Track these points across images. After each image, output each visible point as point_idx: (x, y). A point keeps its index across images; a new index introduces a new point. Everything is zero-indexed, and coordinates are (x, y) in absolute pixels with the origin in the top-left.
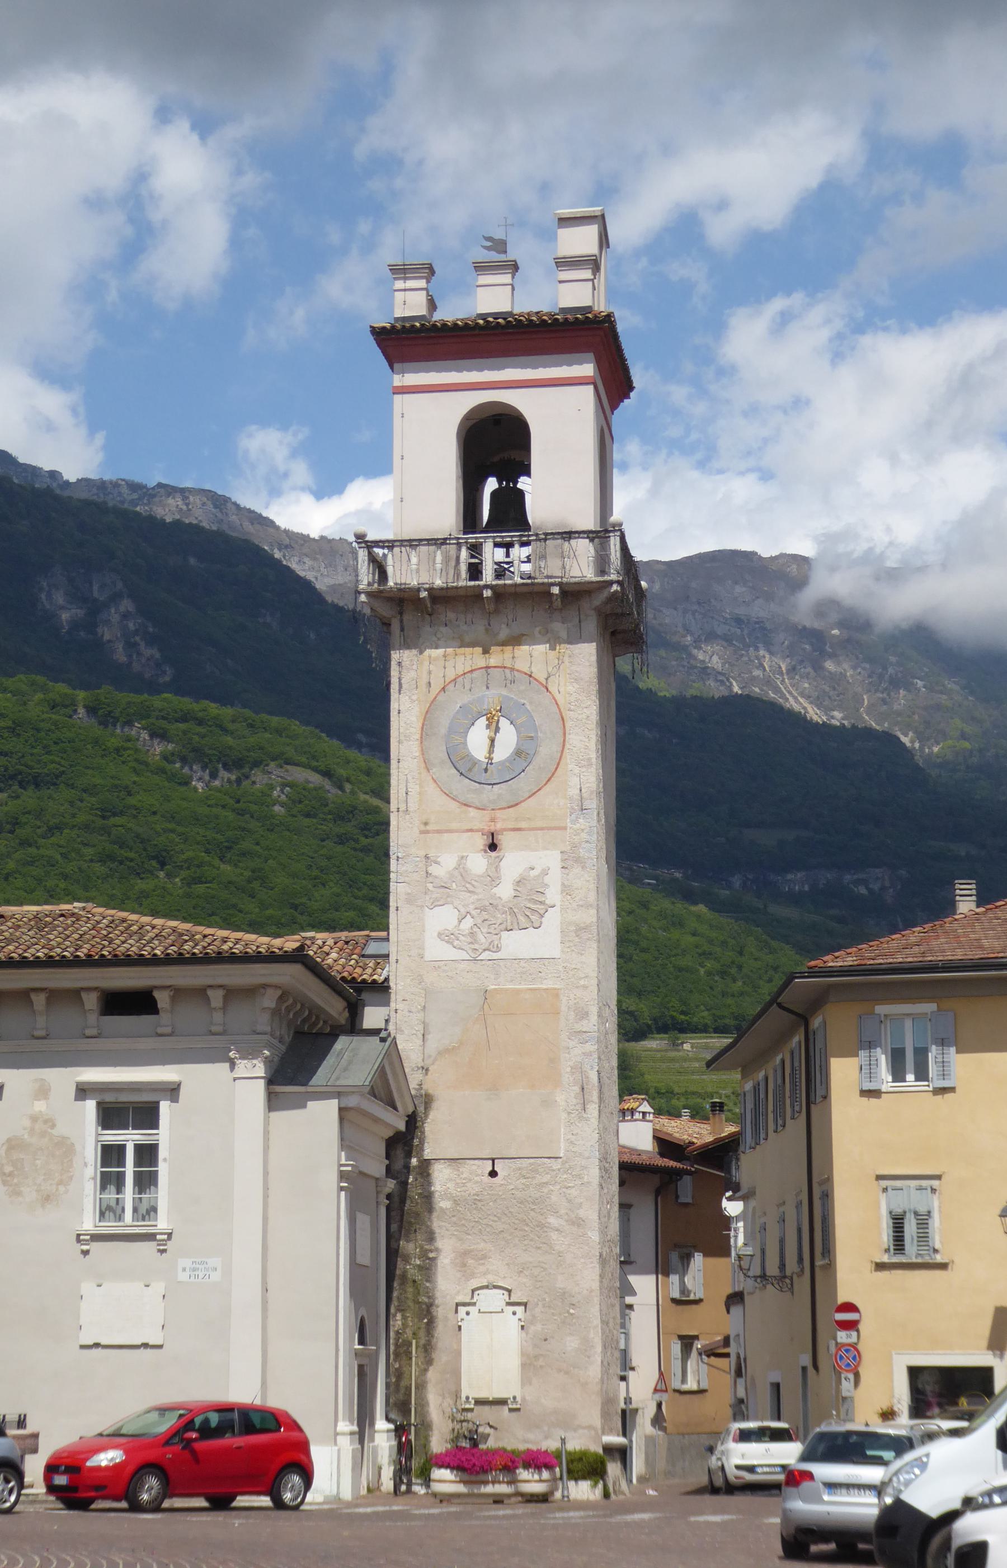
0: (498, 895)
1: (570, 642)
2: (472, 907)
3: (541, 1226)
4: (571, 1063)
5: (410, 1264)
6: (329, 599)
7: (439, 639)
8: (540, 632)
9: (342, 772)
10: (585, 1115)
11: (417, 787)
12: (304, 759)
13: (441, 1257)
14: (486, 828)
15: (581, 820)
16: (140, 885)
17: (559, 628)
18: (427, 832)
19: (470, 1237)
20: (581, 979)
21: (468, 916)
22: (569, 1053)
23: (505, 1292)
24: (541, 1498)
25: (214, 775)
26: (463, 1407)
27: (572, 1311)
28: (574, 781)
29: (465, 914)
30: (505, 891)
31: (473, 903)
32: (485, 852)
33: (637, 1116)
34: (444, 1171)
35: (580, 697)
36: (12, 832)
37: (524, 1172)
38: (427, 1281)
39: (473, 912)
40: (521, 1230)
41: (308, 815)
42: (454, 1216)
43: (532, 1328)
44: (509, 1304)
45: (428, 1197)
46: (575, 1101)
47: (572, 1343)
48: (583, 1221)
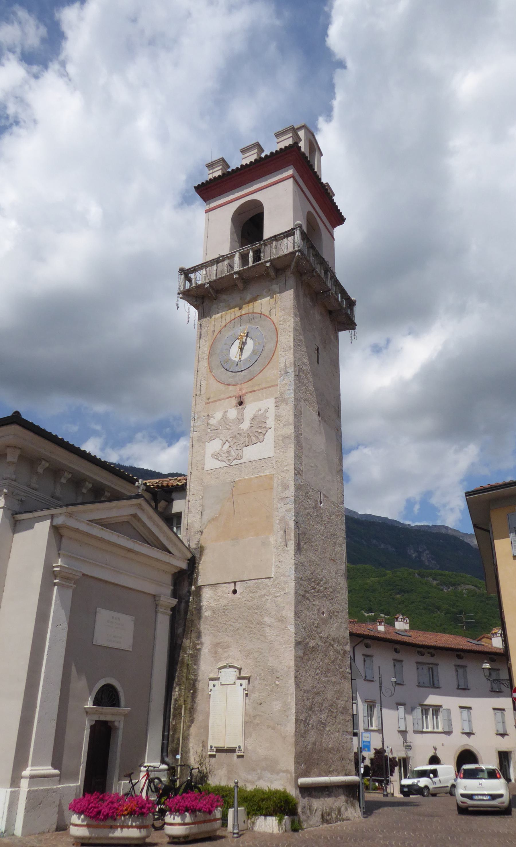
0: (242, 428)
1: (280, 292)
2: (229, 437)
3: (260, 623)
4: (279, 518)
5: (186, 654)
6: (474, 547)
7: (219, 309)
8: (266, 292)
9: (479, 585)
10: (286, 549)
11: (206, 381)
12: (470, 583)
13: (203, 648)
14: (238, 395)
15: (285, 379)
16: (434, 615)
17: (275, 287)
18: (209, 403)
19: (220, 634)
20: (285, 466)
21: (227, 442)
22: (278, 511)
23: (236, 670)
24: (182, 840)
25: (449, 588)
26: (209, 753)
27: (277, 682)
28: (282, 360)
29: (225, 441)
30: (246, 425)
31: (229, 435)
32: (237, 406)
33: (498, 635)
34: (209, 592)
35: (285, 317)
36: (403, 604)
37: (252, 589)
38: (195, 664)
39: (229, 440)
40: (249, 627)
41: (472, 596)
42: (212, 621)
43: (253, 695)
44: (239, 678)
45: (199, 609)
46: (281, 540)
47: (277, 706)
48: (285, 618)
